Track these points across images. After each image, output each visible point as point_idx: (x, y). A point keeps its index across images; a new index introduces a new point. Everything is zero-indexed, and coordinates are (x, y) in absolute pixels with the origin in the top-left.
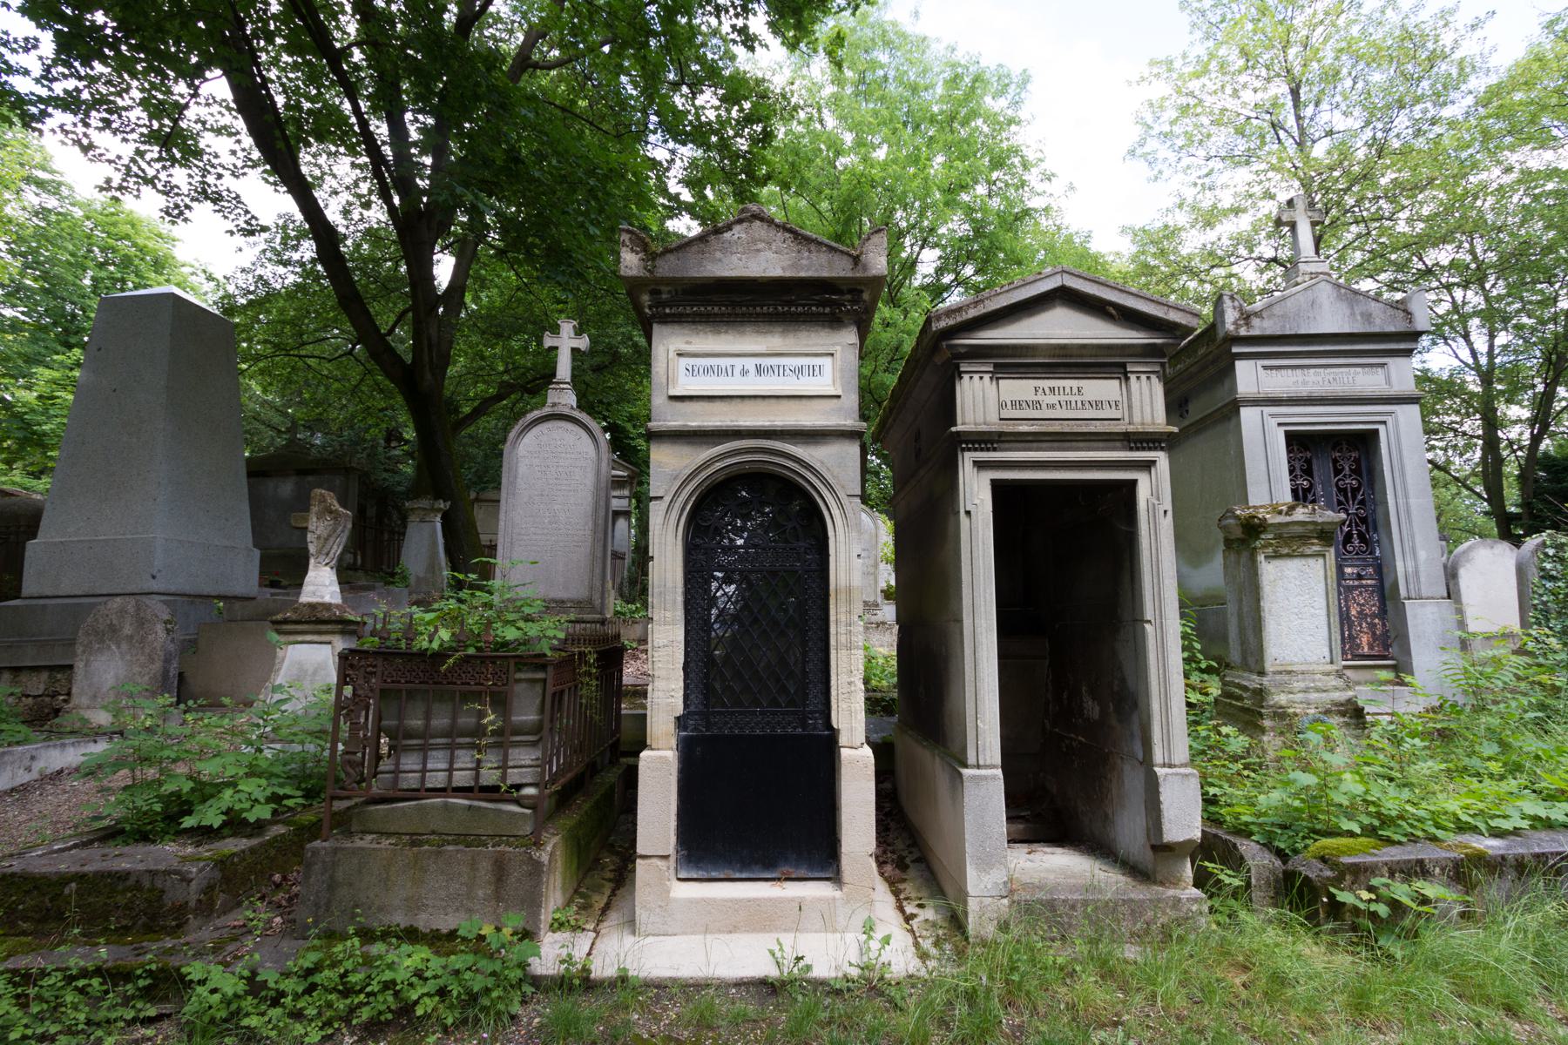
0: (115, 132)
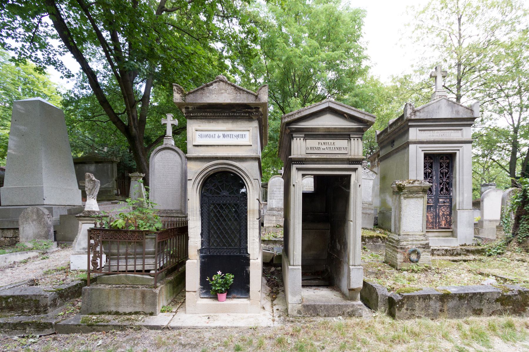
0: (13, 38)
